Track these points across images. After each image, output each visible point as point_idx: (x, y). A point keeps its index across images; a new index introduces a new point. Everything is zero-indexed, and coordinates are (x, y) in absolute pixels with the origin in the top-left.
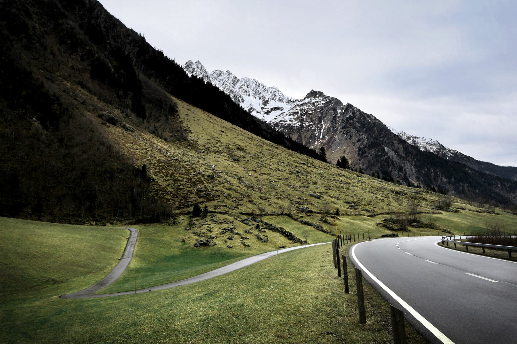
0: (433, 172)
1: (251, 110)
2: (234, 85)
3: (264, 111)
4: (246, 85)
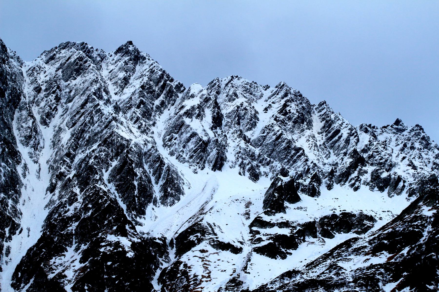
0: (316, 228)
1: (192, 238)
2: (147, 114)
3: (260, 240)
4: (208, 114)
